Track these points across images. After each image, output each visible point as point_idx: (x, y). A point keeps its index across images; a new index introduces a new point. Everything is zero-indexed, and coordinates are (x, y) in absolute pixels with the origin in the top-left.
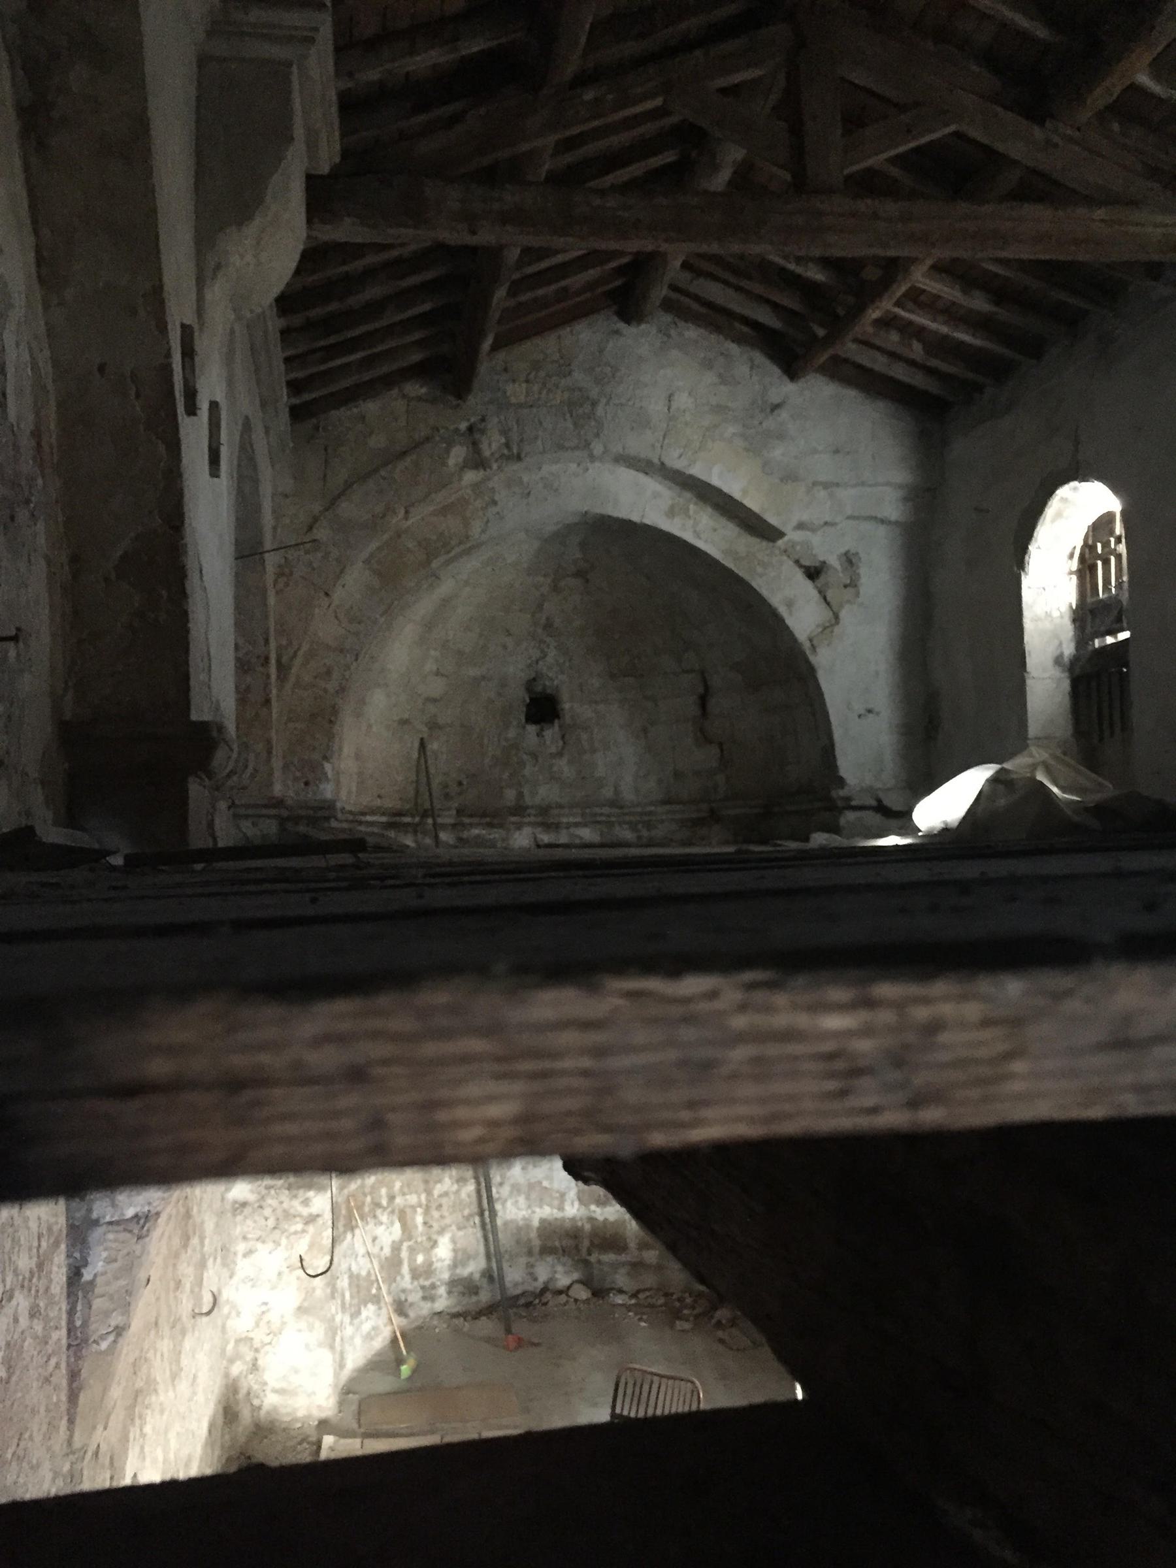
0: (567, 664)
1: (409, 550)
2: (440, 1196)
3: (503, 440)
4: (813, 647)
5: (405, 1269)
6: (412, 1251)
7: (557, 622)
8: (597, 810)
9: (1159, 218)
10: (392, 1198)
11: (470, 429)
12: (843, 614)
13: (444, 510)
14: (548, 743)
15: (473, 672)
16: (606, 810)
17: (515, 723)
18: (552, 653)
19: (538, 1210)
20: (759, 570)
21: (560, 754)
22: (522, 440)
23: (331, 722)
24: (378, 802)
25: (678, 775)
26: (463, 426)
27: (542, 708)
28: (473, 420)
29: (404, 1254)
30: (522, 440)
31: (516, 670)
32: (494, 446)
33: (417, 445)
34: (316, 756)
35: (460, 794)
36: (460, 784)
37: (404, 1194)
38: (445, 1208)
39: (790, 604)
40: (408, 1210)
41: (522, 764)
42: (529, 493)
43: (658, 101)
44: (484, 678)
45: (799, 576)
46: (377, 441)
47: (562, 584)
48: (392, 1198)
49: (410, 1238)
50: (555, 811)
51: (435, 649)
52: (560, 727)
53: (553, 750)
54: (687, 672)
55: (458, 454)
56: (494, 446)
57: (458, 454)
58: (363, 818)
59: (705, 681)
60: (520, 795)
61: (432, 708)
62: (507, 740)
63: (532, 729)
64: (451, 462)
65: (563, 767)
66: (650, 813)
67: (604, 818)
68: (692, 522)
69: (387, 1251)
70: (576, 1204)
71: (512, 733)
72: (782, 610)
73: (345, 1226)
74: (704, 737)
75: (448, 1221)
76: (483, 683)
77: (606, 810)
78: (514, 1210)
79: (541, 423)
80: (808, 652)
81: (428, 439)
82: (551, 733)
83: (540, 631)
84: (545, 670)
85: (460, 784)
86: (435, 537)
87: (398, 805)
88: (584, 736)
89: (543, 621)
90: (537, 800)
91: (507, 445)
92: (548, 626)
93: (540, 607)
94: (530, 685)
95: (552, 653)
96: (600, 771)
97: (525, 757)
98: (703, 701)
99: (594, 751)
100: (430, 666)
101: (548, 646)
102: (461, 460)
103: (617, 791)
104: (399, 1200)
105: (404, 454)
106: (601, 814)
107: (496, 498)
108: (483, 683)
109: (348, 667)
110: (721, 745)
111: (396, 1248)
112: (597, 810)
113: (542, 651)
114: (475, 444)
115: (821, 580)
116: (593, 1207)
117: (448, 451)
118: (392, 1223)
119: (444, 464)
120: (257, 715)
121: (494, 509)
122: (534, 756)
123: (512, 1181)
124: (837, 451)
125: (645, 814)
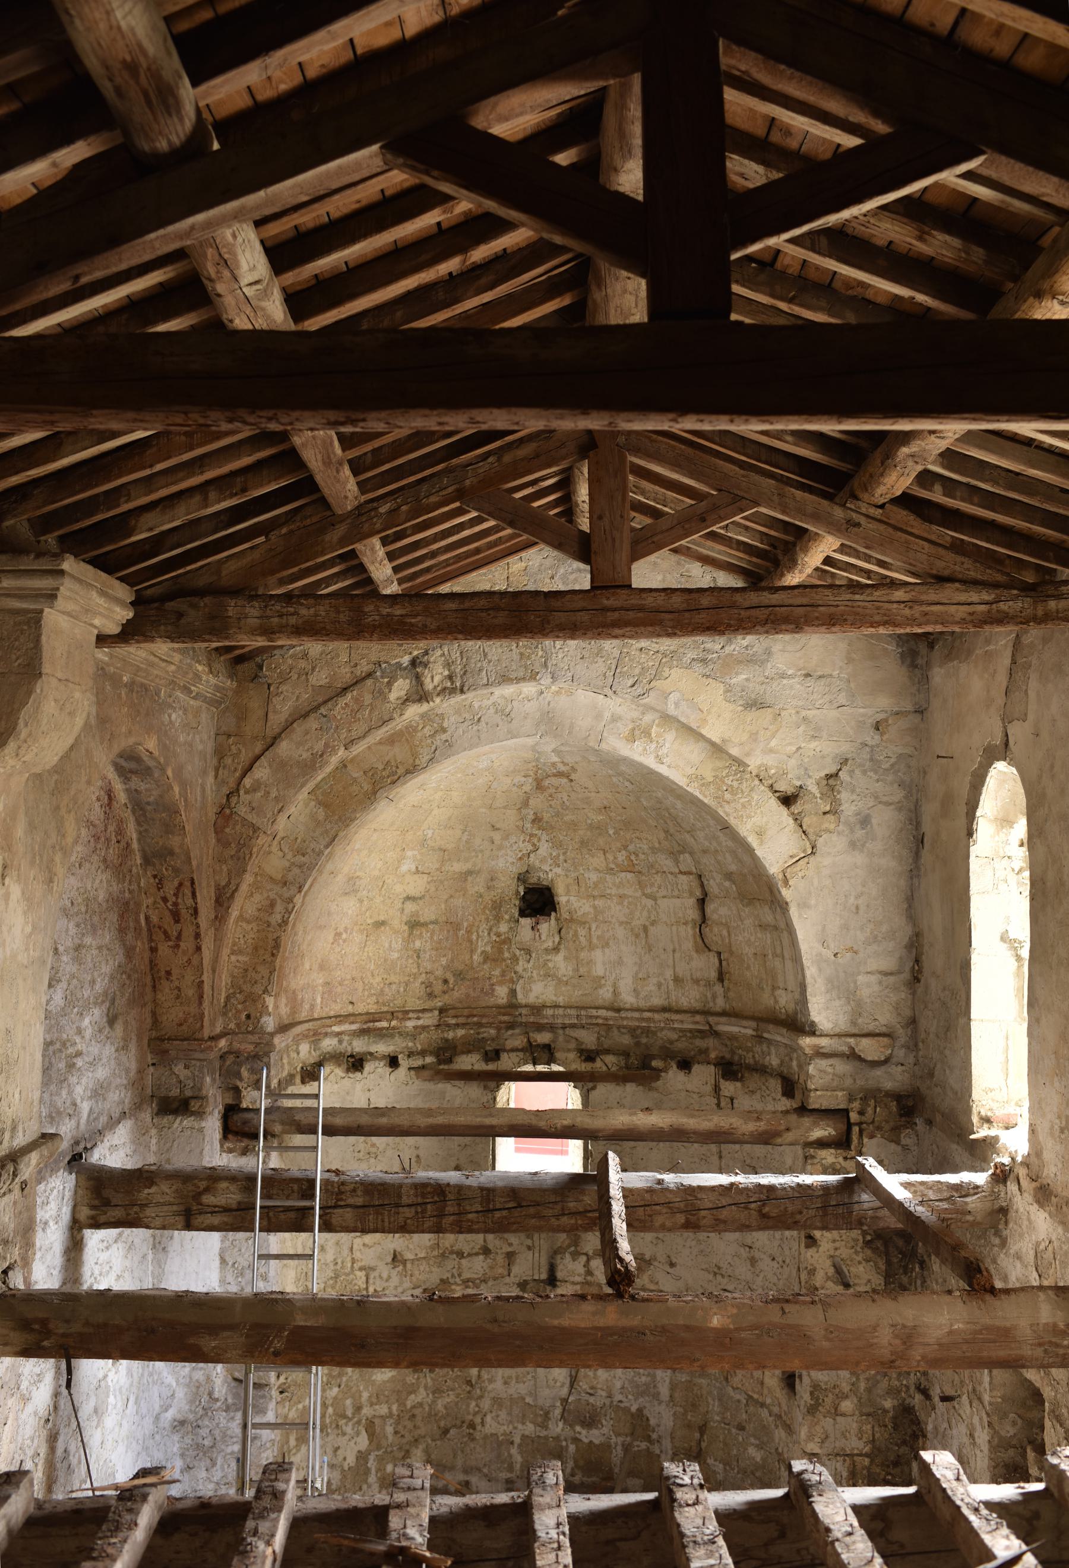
0: (562, 857)
1: (355, 780)
2: (413, 1407)
3: (446, 673)
4: (786, 881)
5: (372, 1479)
6: (380, 1460)
7: (546, 816)
8: (594, 1012)
9: (963, 597)
10: (358, 1409)
11: (414, 663)
12: (820, 842)
13: (391, 740)
14: (543, 937)
15: (458, 867)
16: (603, 1013)
17: (507, 917)
18: (544, 848)
19: (520, 1426)
20: (727, 796)
21: (556, 949)
22: (465, 673)
23: (273, 955)
24: (350, 1009)
25: (677, 980)
26: (406, 660)
27: (538, 901)
28: (415, 653)
29: (372, 1464)
30: (465, 673)
31: (506, 865)
32: (437, 679)
33: (359, 681)
34: (258, 989)
35: (444, 992)
36: (446, 981)
37: (371, 1405)
38: (419, 1418)
39: (760, 834)
40: (377, 1421)
41: (515, 959)
42: (479, 720)
43: (457, 504)
44: (470, 873)
45: (774, 803)
46: (320, 678)
47: (546, 783)
48: (358, 1409)
49: (378, 1448)
50: (549, 1012)
51: (413, 849)
52: (557, 920)
53: (549, 944)
54: (685, 873)
55: (401, 687)
56: (437, 679)
57: (401, 687)
58: (329, 1030)
59: (702, 885)
60: (513, 993)
61: (410, 907)
62: (498, 935)
63: (526, 922)
64: (393, 696)
65: (560, 963)
66: (648, 1020)
67: (600, 1021)
68: (654, 745)
69: (351, 1460)
70: (561, 1424)
71: (503, 928)
72: (752, 840)
73: (297, 1439)
74: (704, 944)
75: (422, 1431)
76: (469, 878)
77: (603, 1013)
78: (494, 1424)
79: (485, 655)
80: (780, 884)
81: (369, 675)
82: (547, 926)
83: (528, 825)
84: (537, 864)
85: (446, 981)
86: (381, 767)
87: (373, 1008)
88: (582, 932)
89: (531, 817)
90: (531, 999)
91: (450, 677)
92: (537, 820)
93: (526, 803)
94: (522, 878)
95: (544, 848)
96: (599, 970)
97: (518, 952)
98: (702, 902)
99: (591, 947)
100: (407, 866)
101: (539, 840)
102: (403, 693)
103: (616, 993)
104: (367, 1411)
105: (345, 690)
106: (597, 1017)
107: (445, 725)
108: (469, 878)
109: (290, 900)
110: (719, 954)
111: (362, 1457)
112: (594, 1012)
113: (534, 845)
114: (418, 677)
115: (796, 808)
116: (578, 1428)
117: (390, 684)
118: (358, 1434)
119: (385, 699)
120: (189, 961)
121: (444, 737)
122: (528, 952)
123: (492, 1395)
124: (808, 675)
125: (643, 1019)
